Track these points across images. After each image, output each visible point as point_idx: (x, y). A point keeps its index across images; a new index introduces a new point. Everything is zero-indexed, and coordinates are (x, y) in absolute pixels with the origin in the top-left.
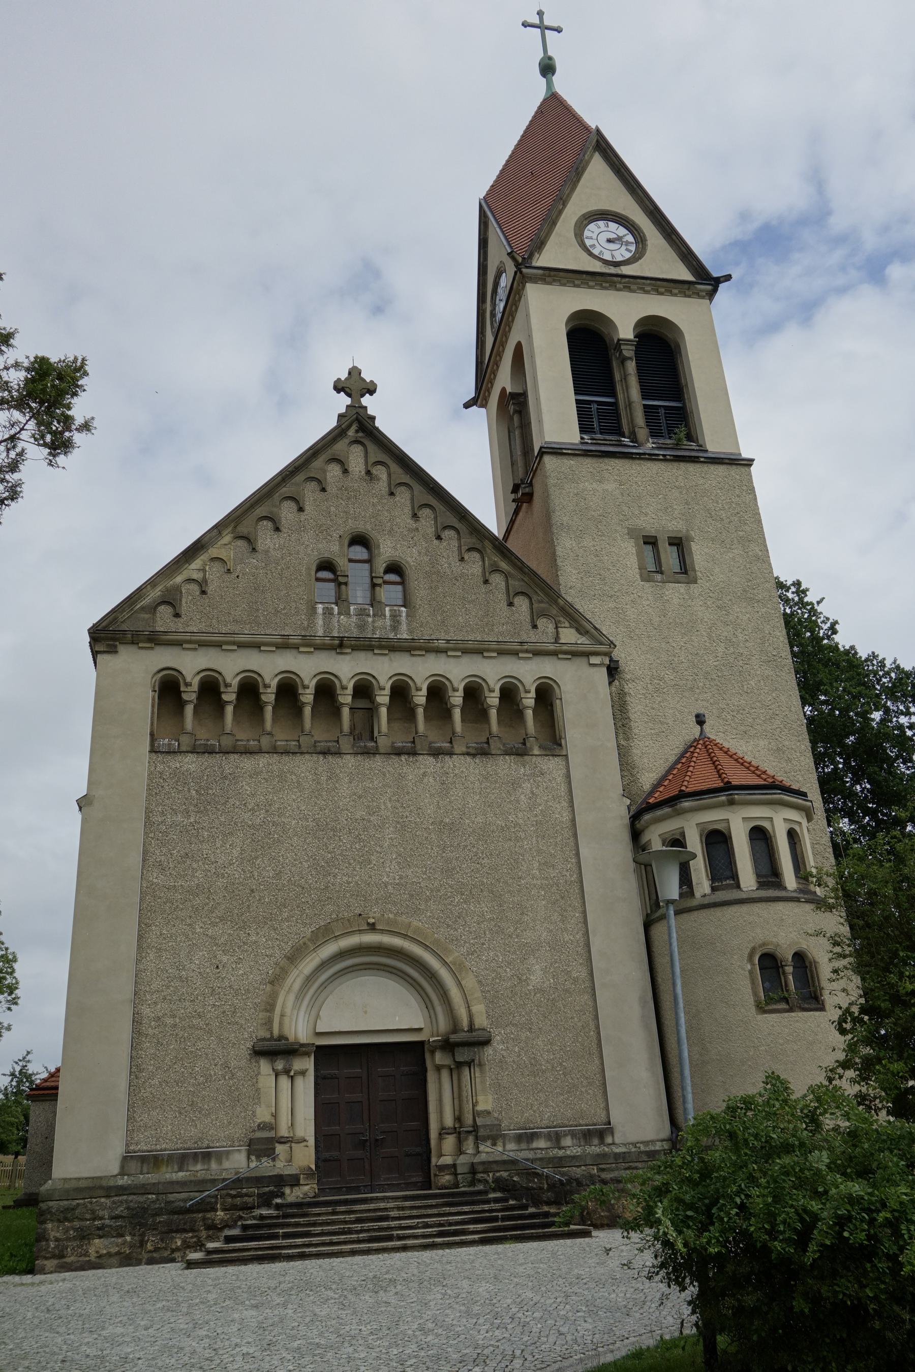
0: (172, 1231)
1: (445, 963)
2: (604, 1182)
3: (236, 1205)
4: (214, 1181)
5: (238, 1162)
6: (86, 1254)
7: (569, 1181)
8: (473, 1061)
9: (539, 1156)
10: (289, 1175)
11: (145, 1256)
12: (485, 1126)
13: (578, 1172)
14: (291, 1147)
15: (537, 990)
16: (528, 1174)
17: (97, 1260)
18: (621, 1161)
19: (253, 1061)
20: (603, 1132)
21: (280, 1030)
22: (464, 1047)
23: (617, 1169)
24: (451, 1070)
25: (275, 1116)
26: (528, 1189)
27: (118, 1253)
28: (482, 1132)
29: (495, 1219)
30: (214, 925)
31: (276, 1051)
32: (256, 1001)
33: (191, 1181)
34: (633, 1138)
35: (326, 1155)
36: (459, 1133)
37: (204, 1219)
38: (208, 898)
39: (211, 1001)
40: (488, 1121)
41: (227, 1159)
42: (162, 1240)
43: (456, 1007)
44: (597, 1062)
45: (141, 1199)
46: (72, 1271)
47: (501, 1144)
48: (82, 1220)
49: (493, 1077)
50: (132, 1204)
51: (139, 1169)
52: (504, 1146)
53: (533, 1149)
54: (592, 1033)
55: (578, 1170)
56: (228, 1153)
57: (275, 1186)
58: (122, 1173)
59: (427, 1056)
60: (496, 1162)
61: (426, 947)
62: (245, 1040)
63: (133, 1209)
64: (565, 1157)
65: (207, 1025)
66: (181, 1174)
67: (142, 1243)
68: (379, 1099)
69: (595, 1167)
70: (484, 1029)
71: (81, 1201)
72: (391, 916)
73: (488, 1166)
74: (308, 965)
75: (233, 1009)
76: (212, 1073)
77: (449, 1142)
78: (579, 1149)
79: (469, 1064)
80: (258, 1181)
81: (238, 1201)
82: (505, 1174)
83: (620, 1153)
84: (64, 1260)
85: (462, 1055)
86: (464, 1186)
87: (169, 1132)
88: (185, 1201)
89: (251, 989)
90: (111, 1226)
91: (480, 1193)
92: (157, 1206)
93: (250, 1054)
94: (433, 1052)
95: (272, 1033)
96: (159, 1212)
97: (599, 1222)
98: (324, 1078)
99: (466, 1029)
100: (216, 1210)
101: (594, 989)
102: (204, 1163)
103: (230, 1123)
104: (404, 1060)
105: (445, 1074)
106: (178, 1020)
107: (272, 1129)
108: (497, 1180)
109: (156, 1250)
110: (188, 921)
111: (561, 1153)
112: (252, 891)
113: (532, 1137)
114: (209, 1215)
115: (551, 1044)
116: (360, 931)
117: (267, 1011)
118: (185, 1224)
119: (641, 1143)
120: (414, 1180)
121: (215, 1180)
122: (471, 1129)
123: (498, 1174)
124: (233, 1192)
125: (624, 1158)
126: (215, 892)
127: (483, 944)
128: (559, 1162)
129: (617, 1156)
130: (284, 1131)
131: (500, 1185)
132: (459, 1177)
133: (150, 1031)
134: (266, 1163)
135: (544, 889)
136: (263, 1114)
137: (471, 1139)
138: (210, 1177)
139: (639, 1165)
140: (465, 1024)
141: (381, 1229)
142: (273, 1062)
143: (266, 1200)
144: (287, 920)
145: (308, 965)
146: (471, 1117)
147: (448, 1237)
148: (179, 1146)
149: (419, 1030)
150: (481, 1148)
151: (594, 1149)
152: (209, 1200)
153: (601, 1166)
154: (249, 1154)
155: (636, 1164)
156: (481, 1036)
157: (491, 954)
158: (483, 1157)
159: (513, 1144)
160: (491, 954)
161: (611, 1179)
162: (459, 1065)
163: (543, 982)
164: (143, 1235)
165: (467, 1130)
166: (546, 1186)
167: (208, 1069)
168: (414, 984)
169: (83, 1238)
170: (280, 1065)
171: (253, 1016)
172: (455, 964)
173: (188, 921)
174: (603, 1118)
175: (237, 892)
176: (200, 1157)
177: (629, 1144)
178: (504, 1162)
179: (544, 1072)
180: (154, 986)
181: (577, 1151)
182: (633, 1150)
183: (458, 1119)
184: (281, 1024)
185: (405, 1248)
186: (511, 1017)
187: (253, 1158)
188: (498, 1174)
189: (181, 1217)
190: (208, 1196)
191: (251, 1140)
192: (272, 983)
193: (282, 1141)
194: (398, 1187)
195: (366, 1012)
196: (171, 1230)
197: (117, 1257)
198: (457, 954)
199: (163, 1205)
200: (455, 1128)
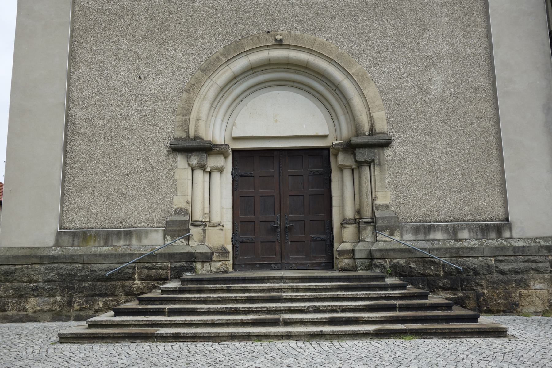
0: (95, 295)
1: (348, 75)
2: (502, 272)
3: (151, 276)
4: (131, 255)
5: (156, 240)
6: (24, 309)
7: (466, 270)
8: (373, 161)
9: (437, 246)
10: (200, 253)
11: (73, 314)
12: (383, 218)
13: (476, 262)
14: (204, 231)
15: (437, 99)
16: (424, 261)
17: (34, 315)
18: (520, 254)
19: (171, 157)
20: (502, 226)
21: (196, 131)
22: (364, 149)
23: (516, 262)
24: (353, 170)
25: (191, 203)
26: (424, 275)
27: (50, 310)
28: (379, 223)
29: (392, 308)
30: (137, 42)
31: (195, 149)
32: (174, 106)
33: (112, 255)
34: (531, 233)
35: (243, 238)
36: (359, 223)
37: (123, 286)
38: (132, 19)
39: (135, 106)
40: (386, 213)
41: (146, 237)
42: (87, 302)
43: (358, 114)
44: (496, 164)
45: (69, 267)
46: (13, 322)
47: (399, 234)
48: (20, 281)
49: (392, 176)
50: (61, 271)
51: (71, 242)
52: (401, 237)
53: (429, 240)
54: (492, 138)
55: (476, 261)
56: (147, 232)
57: (186, 262)
58: (57, 245)
59: (332, 159)
60: (393, 250)
61: (330, 60)
62: (165, 139)
63: (62, 275)
64: (463, 248)
65: (131, 126)
66: (105, 248)
67: (70, 304)
68: (286, 195)
69: (493, 259)
70: (384, 133)
71: (20, 267)
72: (298, 33)
73: (385, 253)
74: (222, 76)
75: (153, 113)
76: (135, 166)
77: (349, 231)
78: (476, 242)
79: (369, 164)
80: (171, 257)
81: (153, 273)
82: (402, 261)
83: (519, 247)
84: (6, 313)
85: (363, 155)
86: (362, 270)
87: (96, 212)
88: (106, 270)
89: (169, 96)
90: (43, 288)
91: (376, 278)
92: (83, 274)
93: (168, 151)
94: (336, 156)
95: (188, 133)
96: (85, 278)
97: (495, 309)
98: (242, 176)
99: (367, 134)
100: (134, 280)
101: (495, 98)
102: (125, 240)
103: (150, 208)
104: (311, 164)
105: (347, 174)
106: (106, 122)
107: (187, 214)
108: (394, 267)
109: (82, 309)
110: (115, 39)
111: (458, 244)
112: (171, 12)
113: (430, 229)
114: (127, 283)
115: (450, 147)
116: (269, 47)
117: (183, 115)
118: (106, 289)
119: (540, 238)
120: (318, 260)
121: (133, 254)
122: (369, 220)
123: (395, 261)
124: (148, 265)
125: (523, 251)
126: (138, 14)
127: (385, 57)
128: (456, 253)
129: (516, 249)
130: (198, 216)
131: (396, 271)
132: (358, 261)
133: (82, 131)
134: (180, 242)
135: (447, 7)
136: (180, 202)
137: (369, 229)
138: (129, 252)
139: (538, 258)
140: (366, 129)
141: (269, 311)
142: (188, 158)
143: (177, 274)
144: (202, 37)
145: (222, 76)
146: (370, 210)
147: (338, 327)
148: (107, 225)
149: (325, 136)
150: (379, 237)
151: (492, 242)
152: (127, 270)
153: (498, 258)
154: (165, 233)
155: (536, 258)
156: (383, 139)
157: (393, 66)
158: (381, 245)
159: (410, 235)
160: (393, 66)
161: (510, 270)
162: (360, 164)
163: (444, 92)
164: (71, 296)
165: (361, 221)
166: (442, 273)
167: (132, 163)
168: (321, 98)
169: (21, 296)
170: (194, 161)
171: (171, 119)
172: (357, 75)
173: (115, 39)
174: (500, 214)
175: (157, 14)
176: (123, 235)
177: (528, 239)
178: (401, 251)
179: (442, 172)
180: (85, 93)
181: (475, 243)
182: (533, 244)
183: (358, 212)
184: (196, 127)
185: (289, 336)
186: (411, 122)
187: (168, 237)
188: (395, 261)
189: (104, 283)
190: (126, 268)
191: (167, 222)
192: (188, 91)
193: (196, 224)
194: (304, 266)
195: (276, 121)
196: (95, 294)
197: (50, 313)
198: (359, 67)
199: (87, 273)
200: (355, 219)
